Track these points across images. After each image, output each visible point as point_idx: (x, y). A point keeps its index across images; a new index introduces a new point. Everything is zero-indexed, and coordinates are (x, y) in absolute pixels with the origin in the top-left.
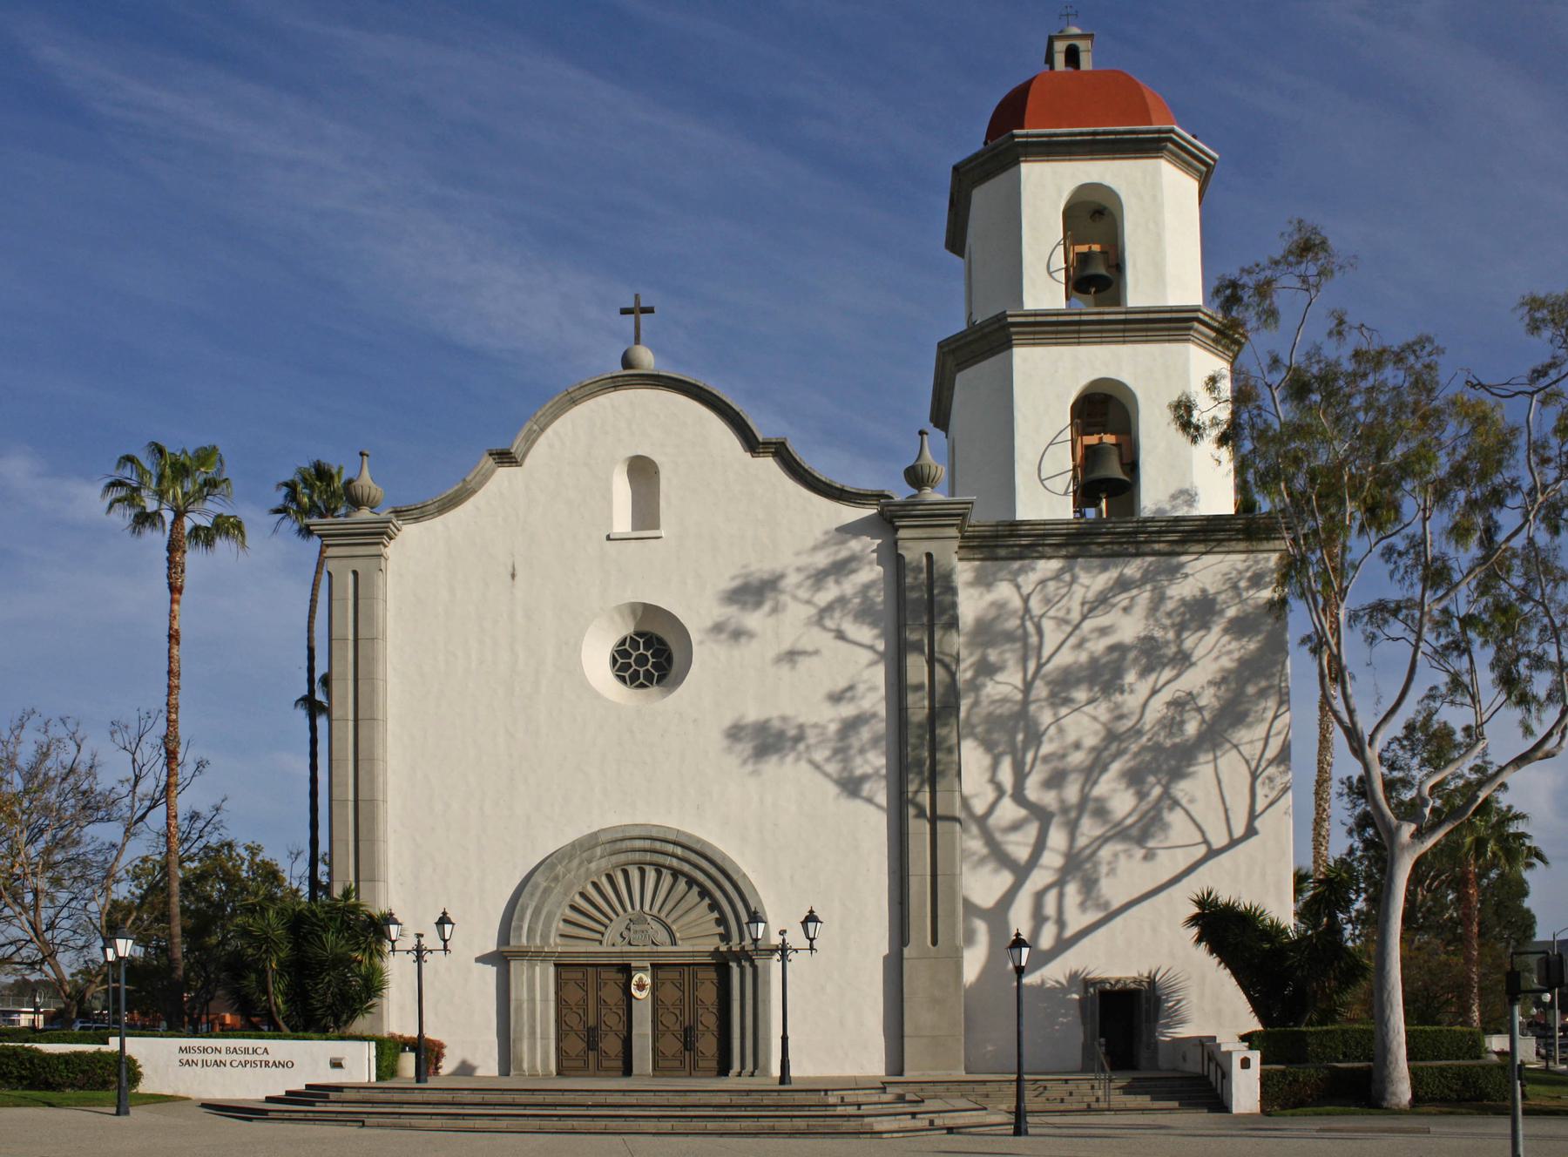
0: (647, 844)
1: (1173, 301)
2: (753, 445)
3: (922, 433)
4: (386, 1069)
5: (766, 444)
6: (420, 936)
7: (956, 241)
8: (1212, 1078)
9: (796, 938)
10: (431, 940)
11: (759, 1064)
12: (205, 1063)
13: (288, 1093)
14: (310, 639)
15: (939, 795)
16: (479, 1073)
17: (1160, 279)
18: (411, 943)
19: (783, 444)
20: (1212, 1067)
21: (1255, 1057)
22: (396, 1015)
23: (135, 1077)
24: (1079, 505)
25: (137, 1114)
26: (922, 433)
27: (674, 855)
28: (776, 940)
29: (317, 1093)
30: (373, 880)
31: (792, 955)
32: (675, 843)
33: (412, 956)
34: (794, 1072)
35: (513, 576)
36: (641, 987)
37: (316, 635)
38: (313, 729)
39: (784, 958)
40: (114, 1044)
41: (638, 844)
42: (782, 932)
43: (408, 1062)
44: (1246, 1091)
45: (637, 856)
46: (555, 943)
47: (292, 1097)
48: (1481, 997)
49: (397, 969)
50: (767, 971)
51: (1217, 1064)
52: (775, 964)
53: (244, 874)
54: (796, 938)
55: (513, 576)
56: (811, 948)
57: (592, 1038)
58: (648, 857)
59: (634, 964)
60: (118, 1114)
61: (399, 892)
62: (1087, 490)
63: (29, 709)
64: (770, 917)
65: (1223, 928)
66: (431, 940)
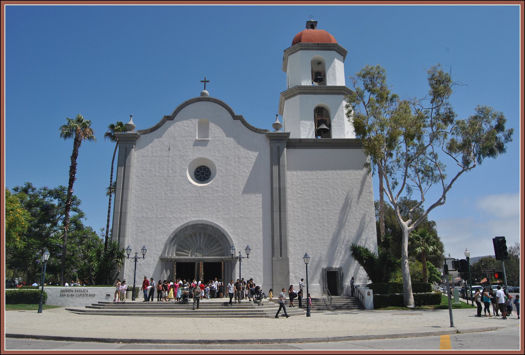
1: (338, 85)
2: (235, 117)
5: (237, 116)
8: (360, 298)
9: (244, 255)
10: (140, 255)
12: (68, 296)
14: (112, 166)
15: (282, 213)
16: (444, 254)
17: (335, 79)
18: (132, 255)
19: (241, 116)
20: (360, 294)
21: (371, 291)
23: (45, 297)
24: (316, 135)
26: (277, 115)
28: (237, 255)
29: (101, 304)
30: (124, 236)
31: (242, 259)
33: (134, 260)
35: (169, 149)
37: (114, 165)
39: (240, 260)
42: (240, 253)
44: (369, 299)
47: (94, 306)
48: (125, 131)
50: (235, 264)
52: (238, 262)
54: (244, 255)
55: (169, 149)
60: (38, 312)
61: (130, 241)
62: (318, 132)
64: (236, 248)
65: (358, 253)
66: (140, 255)
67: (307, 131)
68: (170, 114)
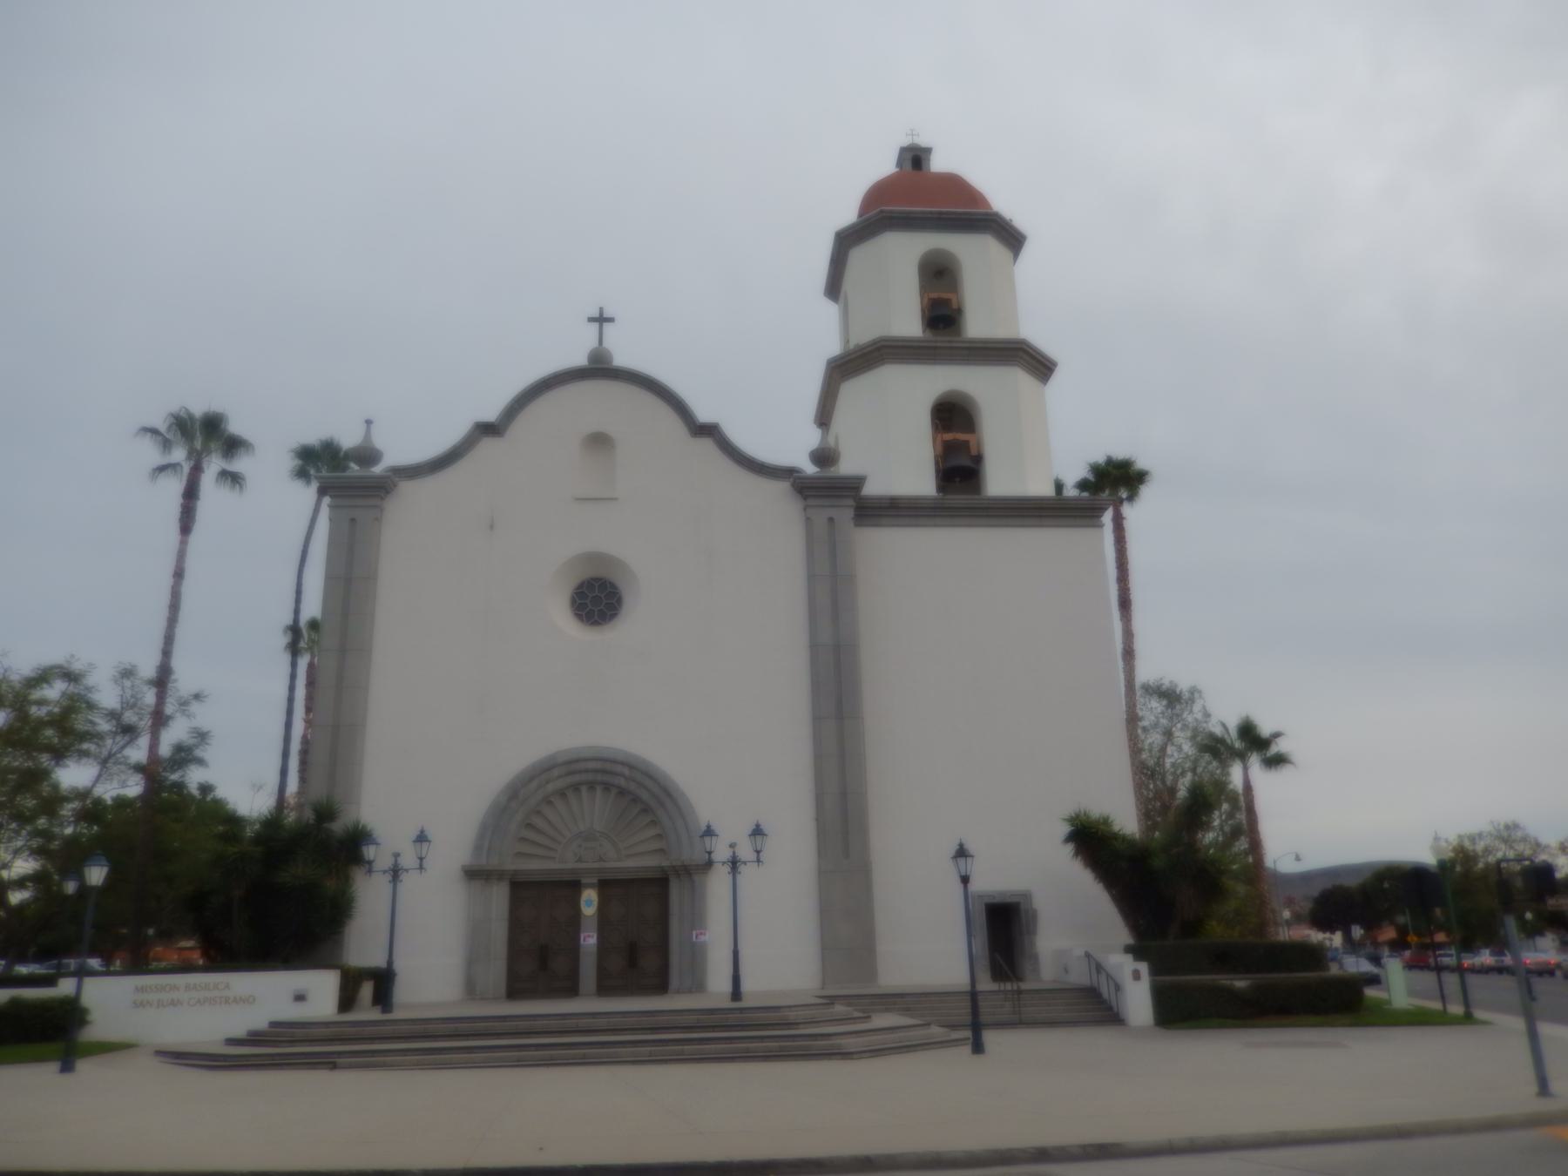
0: (599, 765)
3: (599, 442)
4: (347, 1001)
6: (397, 855)
7: (834, 288)
11: (698, 986)
12: (160, 1004)
13: (274, 1024)
22: (363, 945)
25: (84, 1067)
27: (587, 771)
32: (623, 764)
33: (389, 877)
34: (747, 985)
36: (589, 903)
38: (294, 665)
40: (66, 987)
41: (591, 765)
42: (732, 846)
43: (367, 990)
44: (1138, 999)
45: (590, 777)
46: (511, 865)
47: (255, 1038)
49: (370, 893)
51: (1108, 976)
53: (64, 812)
55: (492, 527)
56: (758, 861)
57: (543, 957)
58: (599, 777)
59: (584, 881)
63: (1280, 746)
67: (910, 471)
68: (488, 445)
